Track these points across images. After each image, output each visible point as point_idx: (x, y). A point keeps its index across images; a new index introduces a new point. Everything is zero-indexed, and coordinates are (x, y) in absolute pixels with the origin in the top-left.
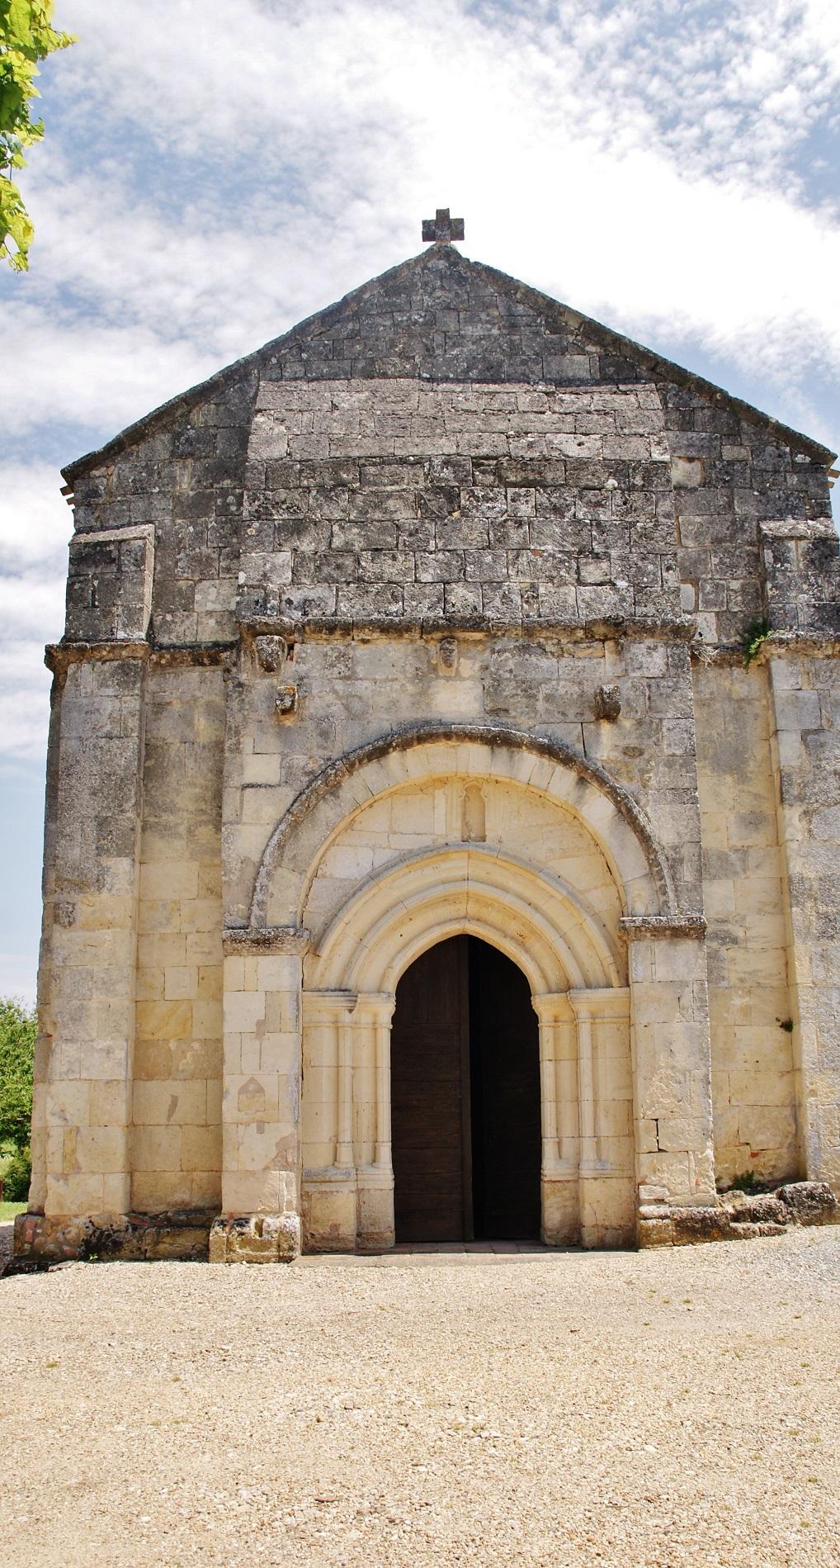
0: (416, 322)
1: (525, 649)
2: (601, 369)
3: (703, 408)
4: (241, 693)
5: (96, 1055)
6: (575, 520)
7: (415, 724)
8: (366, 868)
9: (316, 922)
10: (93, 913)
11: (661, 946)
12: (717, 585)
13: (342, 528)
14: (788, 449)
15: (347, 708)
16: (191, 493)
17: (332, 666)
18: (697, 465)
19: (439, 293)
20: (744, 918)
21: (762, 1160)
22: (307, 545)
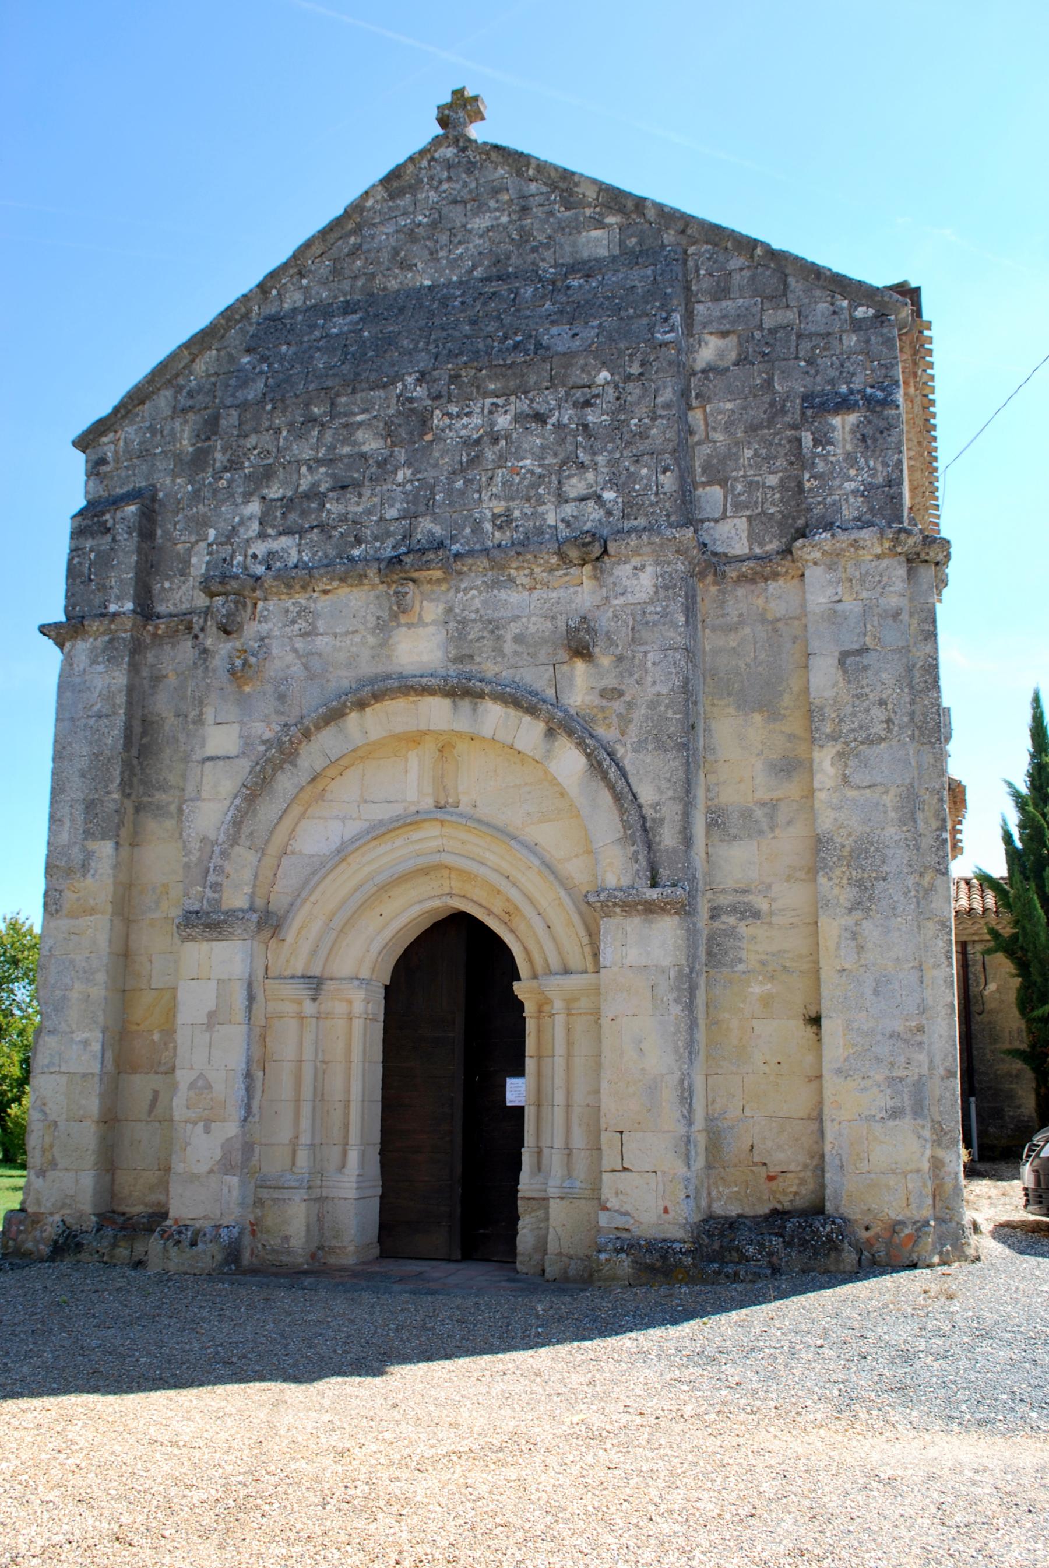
0: (419, 225)
1: (495, 584)
2: (622, 243)
3: (741, 269)
4: (205, 660)
5: (74, 1047)
6: (559, 426)
7: (373, 681)
8: (335, 841)
9: (279, 901)
10: (78, 899)
11: (634, 924)
12: (751, 483)
13: (310, 468)
14: (845, 303)
15: (306, 667)
16: (191, 449)
17: (293, 622)
18: (733, 340)
19: (445, 186)
20: (769, 886)
21: (779, 1184)
22: (275, 492)
